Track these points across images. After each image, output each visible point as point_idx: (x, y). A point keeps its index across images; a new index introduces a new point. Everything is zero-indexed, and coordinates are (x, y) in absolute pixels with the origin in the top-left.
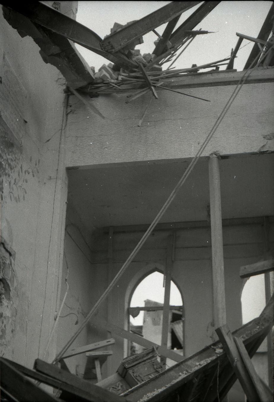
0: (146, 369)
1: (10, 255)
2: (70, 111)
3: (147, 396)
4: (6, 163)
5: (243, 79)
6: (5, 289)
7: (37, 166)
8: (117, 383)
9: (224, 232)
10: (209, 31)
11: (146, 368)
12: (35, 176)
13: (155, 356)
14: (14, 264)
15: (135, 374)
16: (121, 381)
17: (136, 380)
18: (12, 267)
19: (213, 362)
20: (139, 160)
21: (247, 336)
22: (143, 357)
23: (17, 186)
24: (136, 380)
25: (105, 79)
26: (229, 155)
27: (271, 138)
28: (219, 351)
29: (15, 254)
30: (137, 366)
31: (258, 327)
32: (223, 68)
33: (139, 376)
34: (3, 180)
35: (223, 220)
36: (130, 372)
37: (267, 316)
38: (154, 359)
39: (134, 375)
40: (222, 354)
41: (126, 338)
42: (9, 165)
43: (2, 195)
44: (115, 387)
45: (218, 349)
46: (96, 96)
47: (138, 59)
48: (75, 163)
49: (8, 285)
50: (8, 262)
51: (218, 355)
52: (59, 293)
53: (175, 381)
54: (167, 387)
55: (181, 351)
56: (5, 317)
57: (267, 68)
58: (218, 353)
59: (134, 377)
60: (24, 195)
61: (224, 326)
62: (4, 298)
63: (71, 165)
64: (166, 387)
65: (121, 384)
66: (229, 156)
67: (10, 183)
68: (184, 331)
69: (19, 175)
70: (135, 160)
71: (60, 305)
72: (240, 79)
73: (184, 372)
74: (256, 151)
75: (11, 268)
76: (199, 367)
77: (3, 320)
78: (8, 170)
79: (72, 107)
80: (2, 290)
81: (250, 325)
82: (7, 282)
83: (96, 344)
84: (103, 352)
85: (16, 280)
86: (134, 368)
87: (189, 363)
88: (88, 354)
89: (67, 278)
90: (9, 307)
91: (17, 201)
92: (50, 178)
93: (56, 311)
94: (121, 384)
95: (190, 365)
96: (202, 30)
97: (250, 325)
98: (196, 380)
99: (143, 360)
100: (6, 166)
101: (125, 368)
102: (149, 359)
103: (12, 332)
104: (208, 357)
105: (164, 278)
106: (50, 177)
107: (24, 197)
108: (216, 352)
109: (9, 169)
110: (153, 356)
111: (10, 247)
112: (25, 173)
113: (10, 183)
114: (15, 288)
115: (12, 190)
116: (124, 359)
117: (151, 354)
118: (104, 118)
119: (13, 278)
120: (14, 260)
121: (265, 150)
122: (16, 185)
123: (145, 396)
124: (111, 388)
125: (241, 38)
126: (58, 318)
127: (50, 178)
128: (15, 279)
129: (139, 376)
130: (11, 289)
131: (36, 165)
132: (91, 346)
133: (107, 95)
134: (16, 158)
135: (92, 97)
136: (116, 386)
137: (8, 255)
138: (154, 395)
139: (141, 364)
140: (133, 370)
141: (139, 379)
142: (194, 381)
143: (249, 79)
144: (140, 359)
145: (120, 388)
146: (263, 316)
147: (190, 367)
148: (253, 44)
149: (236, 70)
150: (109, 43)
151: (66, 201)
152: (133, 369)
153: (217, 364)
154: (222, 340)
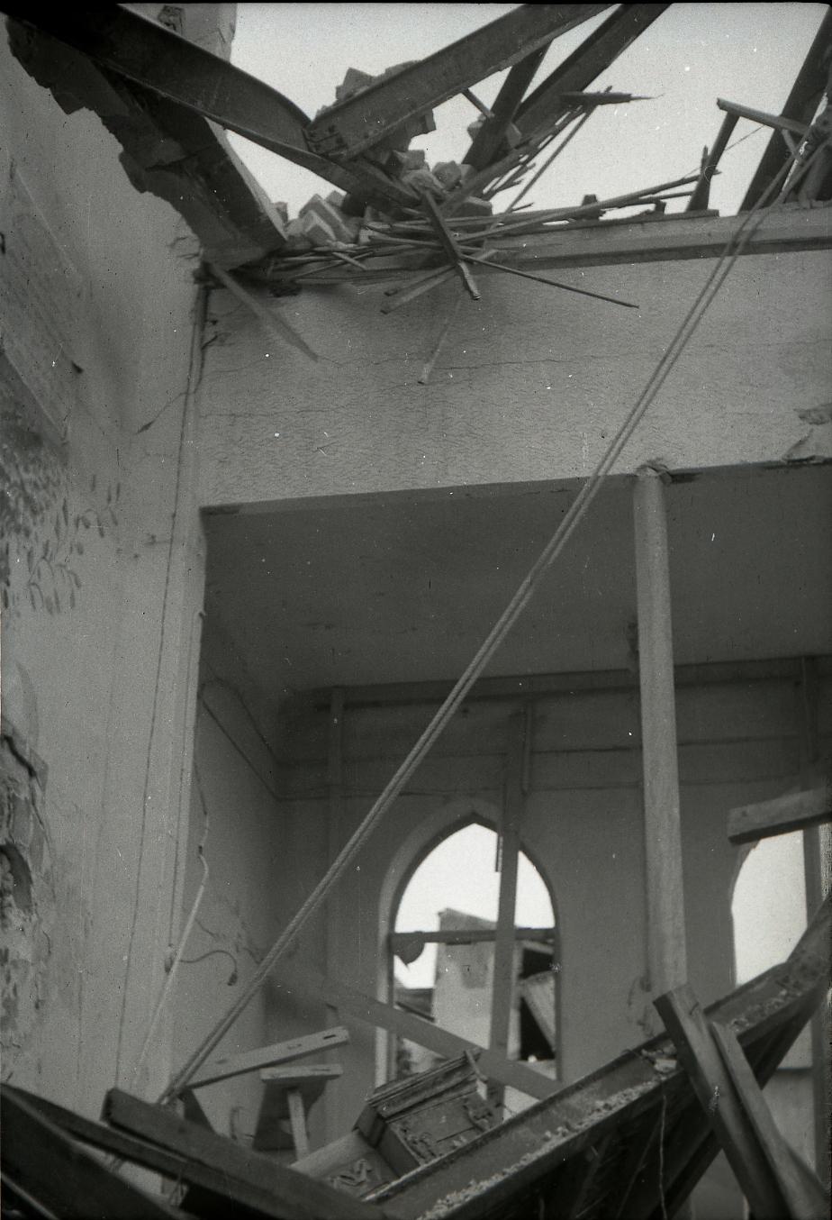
0: (443, 1121)
1: (31, 773)
2: (213, 336)
3: (448, 1201)
4: (17, 494)
5: (739, 240)
6: (15, 878)
7: (113, 504)
8: (355, 1161)
9: (679, 705)
10: (634, 95)
11: (444, 1117)
12: (106, 533)
13: (471, 1079)
14: (43, 802)
15: (410, 1136)
16: (367, 1156)
17: (413, 1153)
18: (36, 810)
19: (645, 1097)
20: (423, 484)
21: (749, 1019)
22: (435, 1084)
23: (53, 564)
24: (413, 1153)
25: (318, 241)
26: (696, 469)
27: (821, 418)
28: (665, 1064)
29: (45, 771)
30: (415, 1111)
31: (784, 992)
32: (677, 206)
33: (421, 1141)
34: (10, 547)
35: (676, 667)
36: (396, 1128)
37: (810, 958)
38: (467, 1089)
39: (406, 1139)
40: (674, 1074)
41: (383, 1026)
42: (28, 500)
43: (5, 593)
44: (349, 1174)
45: (661, 1058)
46: (293, 290)
47: (418, 180)
48: (227, 496)
49: (25, 865)
50: (24, 795)
51: (663, 1078)
52: (180, 889)
53: (531, 1157)
54: (506, 1176)
55: (551, 1066)
56: (15, 963)
57: (812, 207)
58: (662, 1070)
59: (406, 1145)
60: (73, 591)
61: (679, 989)
62: (13, 903)
63: (215, 501)
64: (504, 1174)
65: (367, 1166)
66: (694, 475)
67: (30, 555)
68: (558, 1006)
69: (57, 531)
70: (409, 486)
71: (183, 926)
72: (727, 240)
73: (560, 1129)
74: (776, 458)
75: (34, 812)
76: (605, 1114)
77: (9, 972)
78: (24, 517)
79: (218, 324)
80: (7, 880)
81: (758, 987)
82: (21, 857)
83: (290, 1043)
84: (312, 1067)
85: (49, 849)
86: (406, 1117)
87: (574, 1101)
88: (266, 1074)
89: (203, 845)
90: (28, 930)
91: (50, 611)
92: (152, 541)
93: (170, 945)
94: (367, 1166)
95: (578, 1107)
96: (613, 91)
97: (758, 987)
98: (596, 1154)
99: (433, 1094)
100: (17, 502)
101: (379, 1117)
102: (453, 1088)
103: (37, 1007)
104: (633, 1084)
105: (498, 842)
106: (153, 537)
107: (72, 598)
108: (657, 1067)
109: (28, 514)
110: (465, 1079)
111: (31, 751)
112: (77, 525)
113: (30, 555)
114: (46, 874)
115: (36, 577)
116: (376, 1091)
117: (459, 1073)
118: (314, 357)
119: (41, 844)
120: (43, 788)
121: (805, 456)
122: (49, 562)
123: (439, 1201)
124: (339, 1178)
125: (733, 114)
126: (176, 964)
127: (152, 541)
128: (45, 847)
129: (421, 1141)
130: (34, 876)
131: (109, 500)
132: (278, 1051)
133: (325, 289)
134: (48, 478)
135: (278, 296)
136: (352, 1171)
137: (24, 773)
138: (468, 1200)
139: (427, 1105)
140: (405, 1123)
141: (423, 1150)
142: (589, 1158)
143: (757, 238)
144: (425, 1088)
145: (364, 1176)
146: (797, 960)
147: (578, 1115)
148: (767, 133)
149: (715, 213)
150: (331, 129)
151: (201, 609)
152: (404, 1120)
153: (660, 1104)
154: (674, 1032)
